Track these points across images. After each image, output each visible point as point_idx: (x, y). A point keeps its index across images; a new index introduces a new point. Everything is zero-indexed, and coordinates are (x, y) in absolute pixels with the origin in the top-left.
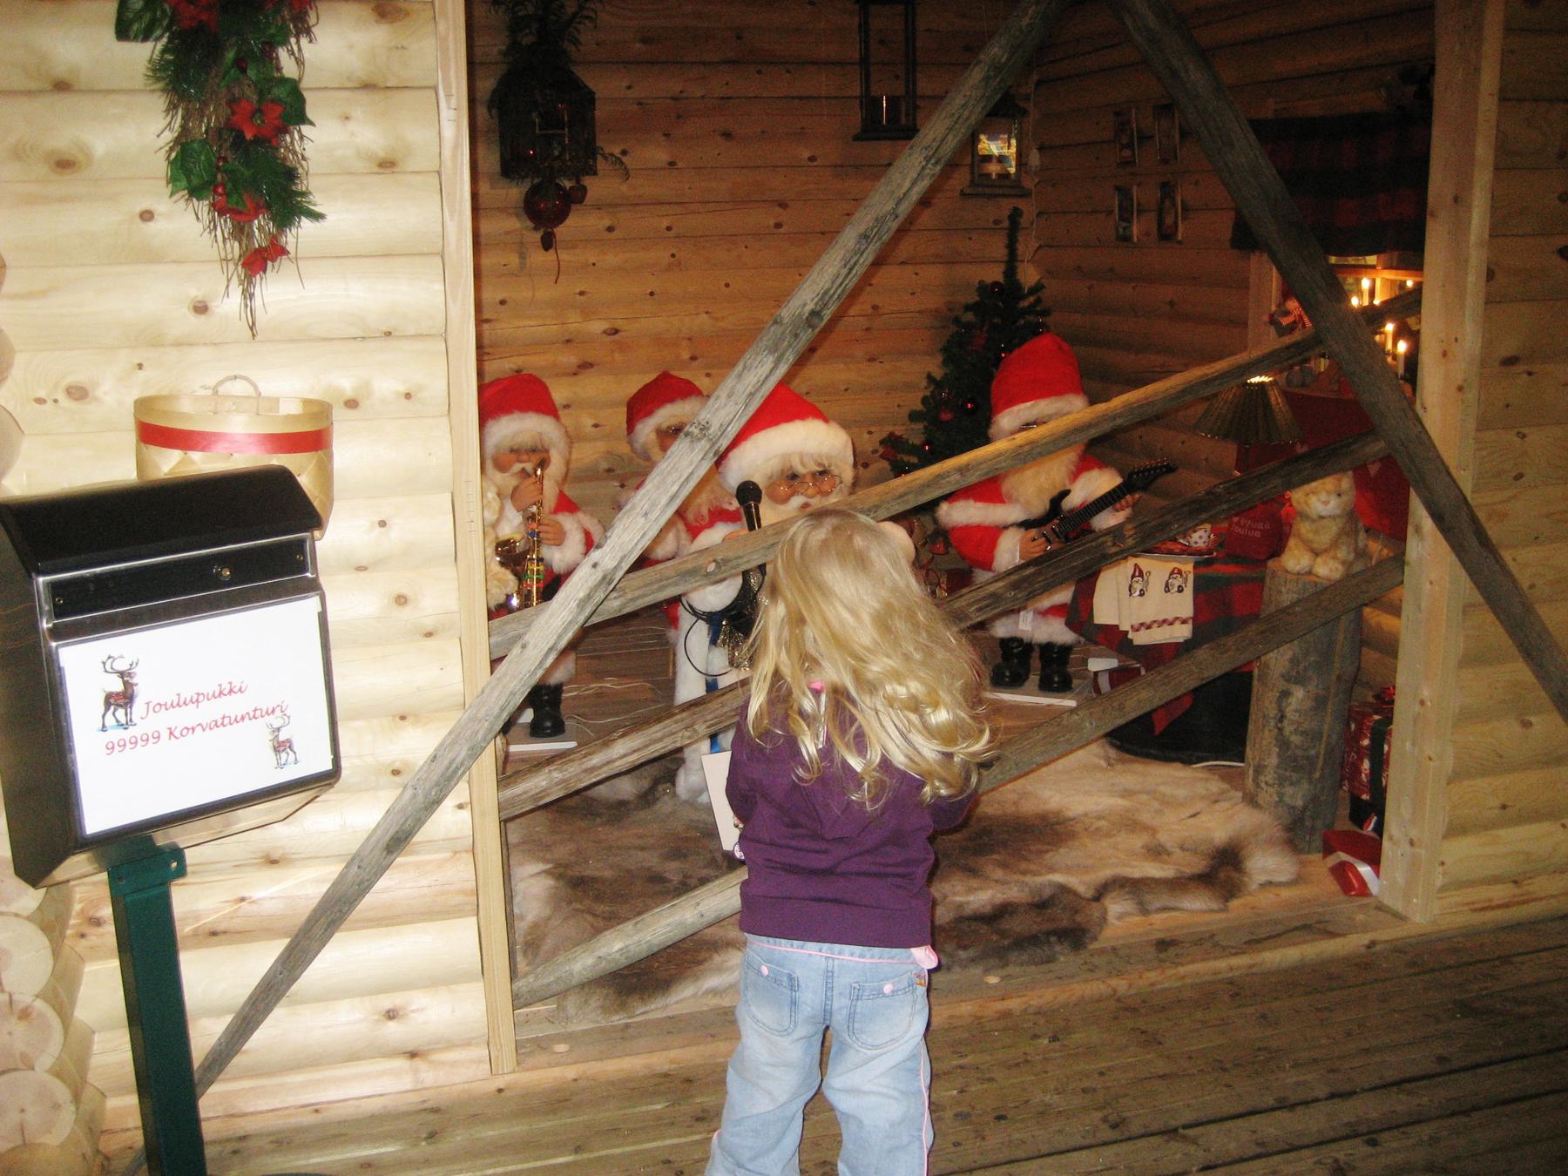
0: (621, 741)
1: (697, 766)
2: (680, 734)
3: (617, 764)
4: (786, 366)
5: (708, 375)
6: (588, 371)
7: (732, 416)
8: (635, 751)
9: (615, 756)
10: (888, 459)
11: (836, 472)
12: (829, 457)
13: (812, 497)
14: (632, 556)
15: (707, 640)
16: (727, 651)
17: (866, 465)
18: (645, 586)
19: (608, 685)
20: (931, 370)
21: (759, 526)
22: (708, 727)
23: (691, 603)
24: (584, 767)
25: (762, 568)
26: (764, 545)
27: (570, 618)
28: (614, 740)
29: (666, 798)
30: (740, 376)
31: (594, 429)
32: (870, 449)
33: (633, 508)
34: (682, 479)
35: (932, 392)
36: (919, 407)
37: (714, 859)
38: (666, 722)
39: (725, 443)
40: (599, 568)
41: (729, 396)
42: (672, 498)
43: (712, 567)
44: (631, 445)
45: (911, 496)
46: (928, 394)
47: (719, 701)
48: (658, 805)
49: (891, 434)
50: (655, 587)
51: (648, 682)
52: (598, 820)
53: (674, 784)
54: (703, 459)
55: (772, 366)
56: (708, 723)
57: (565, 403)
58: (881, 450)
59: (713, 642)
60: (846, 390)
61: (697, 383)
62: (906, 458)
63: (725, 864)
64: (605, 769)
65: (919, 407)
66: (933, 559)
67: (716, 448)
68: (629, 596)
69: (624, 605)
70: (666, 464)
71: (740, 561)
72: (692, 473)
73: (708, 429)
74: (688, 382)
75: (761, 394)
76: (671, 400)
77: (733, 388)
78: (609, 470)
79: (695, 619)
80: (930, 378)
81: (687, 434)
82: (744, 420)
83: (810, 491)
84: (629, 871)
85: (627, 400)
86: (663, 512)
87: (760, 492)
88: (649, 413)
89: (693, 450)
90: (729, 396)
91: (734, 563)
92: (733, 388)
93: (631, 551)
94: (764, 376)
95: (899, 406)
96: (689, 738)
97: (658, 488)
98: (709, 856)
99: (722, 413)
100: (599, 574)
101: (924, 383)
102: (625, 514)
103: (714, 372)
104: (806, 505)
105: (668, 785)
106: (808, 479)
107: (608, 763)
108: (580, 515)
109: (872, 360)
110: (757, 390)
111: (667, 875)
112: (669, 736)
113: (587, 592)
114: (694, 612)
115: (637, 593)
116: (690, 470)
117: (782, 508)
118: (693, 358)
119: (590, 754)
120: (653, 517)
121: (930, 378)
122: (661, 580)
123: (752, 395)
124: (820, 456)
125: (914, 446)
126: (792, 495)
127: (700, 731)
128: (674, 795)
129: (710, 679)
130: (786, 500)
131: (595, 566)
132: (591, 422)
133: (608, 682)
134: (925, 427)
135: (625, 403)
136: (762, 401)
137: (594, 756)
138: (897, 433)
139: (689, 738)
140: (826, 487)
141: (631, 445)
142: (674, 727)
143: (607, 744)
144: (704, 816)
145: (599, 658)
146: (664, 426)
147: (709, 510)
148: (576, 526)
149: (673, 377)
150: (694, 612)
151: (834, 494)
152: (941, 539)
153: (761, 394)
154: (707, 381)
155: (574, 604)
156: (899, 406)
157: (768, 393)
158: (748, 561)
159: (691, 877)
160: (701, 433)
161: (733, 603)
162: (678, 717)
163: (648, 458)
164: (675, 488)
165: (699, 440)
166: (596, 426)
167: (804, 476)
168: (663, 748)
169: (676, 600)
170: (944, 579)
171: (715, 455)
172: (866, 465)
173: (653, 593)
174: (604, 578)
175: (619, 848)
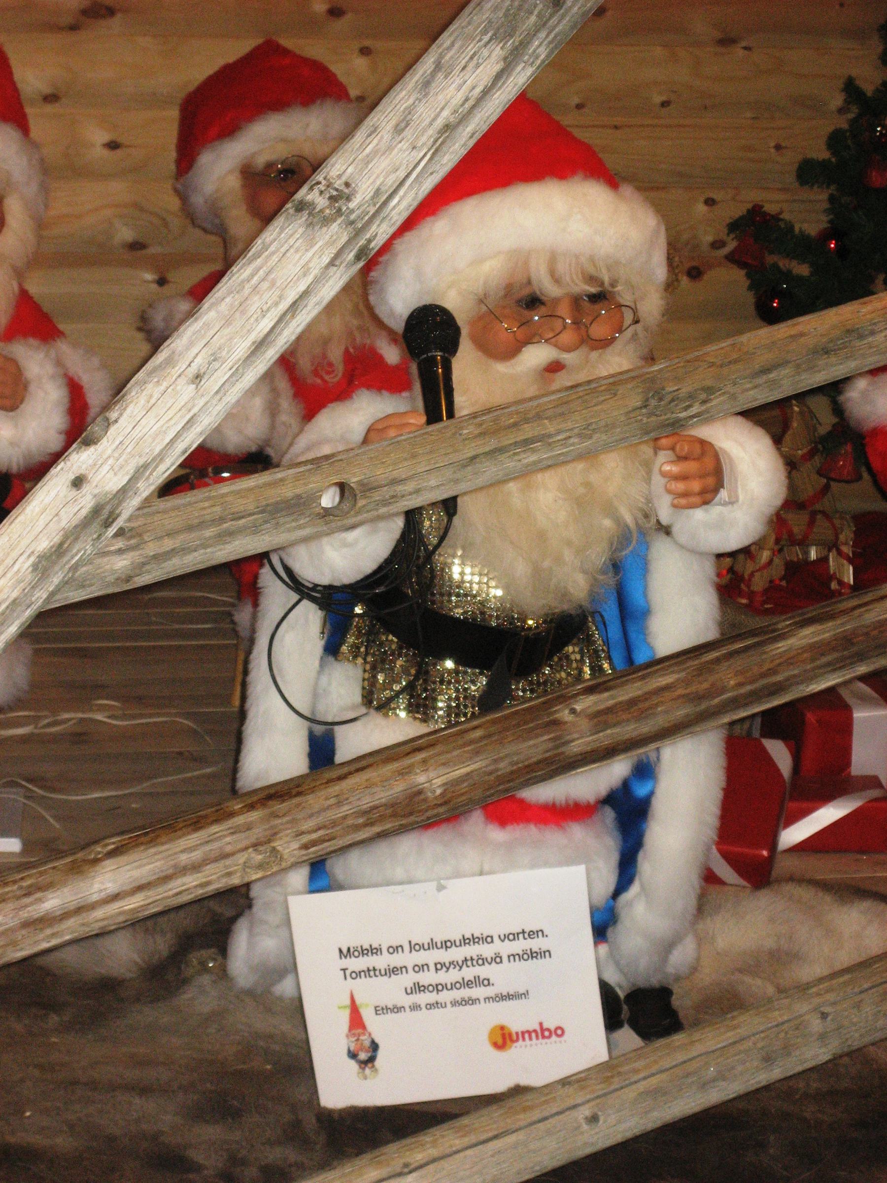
0: (110, 864)
1: (274, 918)
2: (241, 858)
3: (99, 913)
4: (529, 71)
5: (365, 51)
6: (103, 23)
7: (402, 174)
8: (140, 888)
9: (95, 897)
10: (741, 265)
11: (626, 298)
12: (613, 265)
13: (568, 350)
14: (162, 468)
15: (317, 645)
16: (360, 671)
17: (695, 274)
18: (190, 528)
19: (99, 717)
20: (854, 73)
21: (451, 415)
22: (305, 847)
23: (290, 563)
24: (24, 915)
25: (450, 506)
26: (454, 458)
27: (15, 595)
28: (96, 861)
29: (206, 980)
30: (427, 84)
31: (106, 152)
32: (710, 238)
33: (170, 362)
34: (284, 306)
35: (853, 122)
36: (821, 153)
37: (297, 1124)
38: (215, 828)
39: (381, 232)
40: (86, 489)
41: (399, 130)
42: (260, 345)
43: (328, 500)
44: (183, 197)
45: (785, 371)
46: (845, 126)
47: (335, 789)
48: (188, 995)
49: (756, 211)
50: (209, 533)
51: (188, 715)
52: (54, 1019)
53: (223, 950)
54: (332, 263)
55: (498, 67)
56: (305, 839)
57: (47, 90)
58: (732, 245)
59: (332, 649)
60: (665, 104)
61: (338, 69)
62: (784, 263)
63: (322, 1138)
64: (71, 922)
65: (821, 153)
66: (826, 488)
67: (362, 242)
68: (151, 549)
69: (139, 567)
70: (248, 271)
71: (400, 488)
72: (305, 294)
73: (349, 199)
74: (319, 69)
75: (470, 129)
76: (278, 105)
77: (410, 111)
78: (136, 246)
79: (295, 597)
80: (851, 88)
81: (301, 207)
82: (429, 184)
83: (567, 337)
84: (111, 1139)
85: (183, 95)
86: (236, 374)
87: (457, 331)
88: (229, 131)
89: (311, 243)
90: (399, 130)
91: (386, 492)
92: (410, 111)
93: (160, 457)
94: (478, 90)
95: (778, 147)
96: (260, 866)
97: (228, 321)
98: (288, 1117)
99: (382, 164)
100: (86, 501)
101: (838, 100)
102: (150, 374)
103: (378, 45)
104: (555, 367)
105: (212, 951)
106: (564, 310)
107: (79, 910)
108: (63, 347)
109: (727, 41)
110: (464, 119)
111: (192, 1154)
112: (216, 860)
113: (57, 540)
114: (294, 583)
115: (168, 544)
116: (302, 288)
117: (501, 368)
118: (335, 12)
119: (40, 888)
120: (213, 383)
121: (851, 88)
122: (222, 520)
123: (448, 128)
124: (592, 260)
125: (804, 238)
126: (528, 341)
127: (286, 852)
128: (223, 973)
129: (319, 729)
130: (512, 352)
131: (78, 482)
132: (105, 137)
133: (101, 708)
134: (832, 199)
135: (179, 101)
136: (471, 143)
137: (49, 894)
138: (771, 208)
139: (260, 866)
140: (598, 330)
141: (183, 197)
142: (229, 842)
143: (78, 869)
144: (286, 1027)
145: (82, 653)
146: (261, 161)
147: (347, 351)
148: (50, 369)
149: (286, 52)
150: (294, 583)
151: (618, 346)
152: (849, 448)
153: (470, 129)
154: (361, 63)
155: (25, 565)
156: (778, 147)
157: (485, 128)
158: (417, 491)
159: (244, 1162)
160: (330, 206)
161: (380, 568)
162: (240, 820)
163: (221, 232)
164: (266, 324)
165: (326, 221)
166: (113, 146)
167: (556, 301)
168: (202, 885)
169: (262, 558)
170: (847, 535)
171: (358, 258)
172: (695, 274)
173: (204, 546)
174: (96, 511)
175: (93, 1085)
